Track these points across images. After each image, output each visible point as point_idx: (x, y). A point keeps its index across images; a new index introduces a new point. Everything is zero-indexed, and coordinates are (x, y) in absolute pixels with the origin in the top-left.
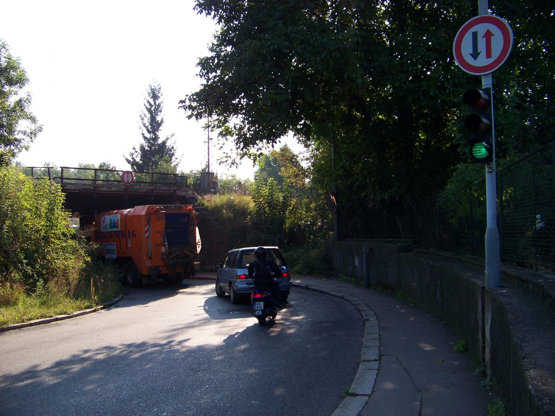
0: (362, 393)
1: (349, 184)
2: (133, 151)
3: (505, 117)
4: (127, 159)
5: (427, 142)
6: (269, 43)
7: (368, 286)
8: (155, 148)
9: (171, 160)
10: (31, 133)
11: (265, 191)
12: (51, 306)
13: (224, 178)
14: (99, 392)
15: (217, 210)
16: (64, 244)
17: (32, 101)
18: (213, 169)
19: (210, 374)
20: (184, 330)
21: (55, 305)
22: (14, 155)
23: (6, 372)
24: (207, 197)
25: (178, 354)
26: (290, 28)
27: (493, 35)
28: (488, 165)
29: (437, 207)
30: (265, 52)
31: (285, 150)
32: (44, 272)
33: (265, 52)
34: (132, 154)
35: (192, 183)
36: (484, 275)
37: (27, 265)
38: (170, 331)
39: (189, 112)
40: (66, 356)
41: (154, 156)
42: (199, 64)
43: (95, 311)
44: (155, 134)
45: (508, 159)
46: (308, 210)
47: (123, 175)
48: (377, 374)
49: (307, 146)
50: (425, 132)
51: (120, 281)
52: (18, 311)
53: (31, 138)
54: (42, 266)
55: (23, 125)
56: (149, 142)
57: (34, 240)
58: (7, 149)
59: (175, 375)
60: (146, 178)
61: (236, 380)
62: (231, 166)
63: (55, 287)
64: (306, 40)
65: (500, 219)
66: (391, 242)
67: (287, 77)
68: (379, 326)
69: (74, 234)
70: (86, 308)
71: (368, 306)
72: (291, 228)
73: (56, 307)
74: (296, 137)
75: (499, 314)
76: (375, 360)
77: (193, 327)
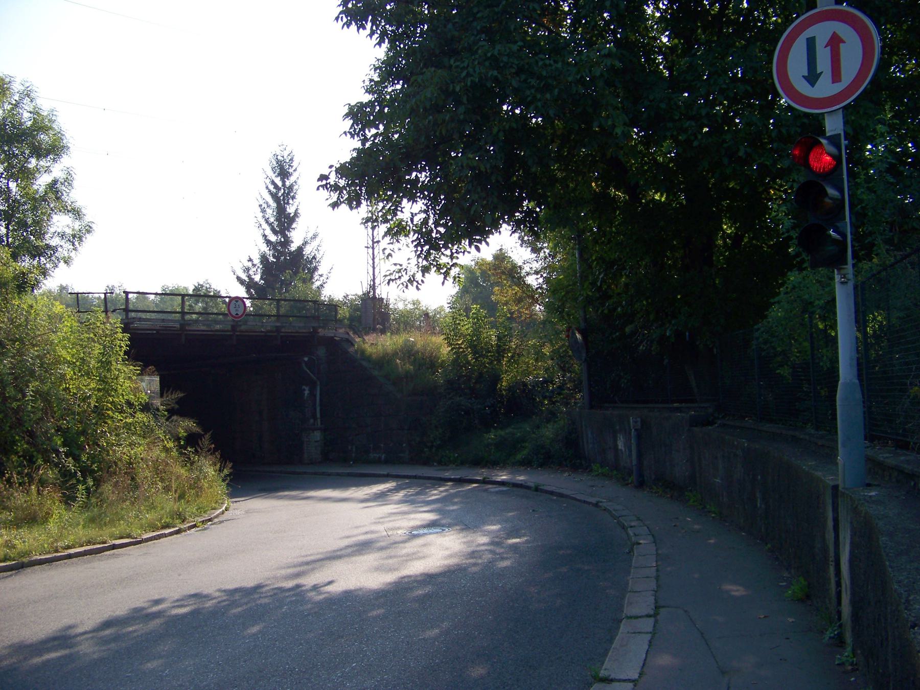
0: (622, 677)
1: (606, 311)
2: (250, 264)
3: (868, 188)
4: (239, 278)
5: (737, 238)
6: (464, 74)
7: (641, 484)
8: (285, 259)
9: (312, 277)
10: (74, 236)
11: (466, 327)
12: (105, 524)
13: (401, 306)
14: (167, 675)
15: (384, 361)
16: (130, 420)
17: (75, 184)
18: (383, 291)
19: (361, 643)
20: (325, 562)
21: (112, 522)
22: (45, 273)
23: (16, 640)
24: (370, 338)
25: (309, 606)
26: (498, 47)
27: (844, 42)
28: (839, 270)
29: (754, 347)
30: (458, 89)
31: (501, 257)
32: (95, 467)
33: (458, 89)
34: (247, 270)
35: (347, 315)
36: (837, 464)
37: (67, 456)
38: (300, 566)
39: (334, 197)
40: (121, 610)
41: (282, 271)
42: (347, 115)
43: (178, 532)
44: (285, 236)
45: (875, 260)
46: (539, 356)
47: (230, 301)
48: (650, 642)
49: (535, 250)
50: (733, 220)
51: (224, 480)
52: (49, 534)
53: (73, 245)
54: (92, 458)
55: (60, 222)
56: (275, 248)
57: (78, 414)
58: (35, 262)
59: (301, 644)
60: (269, 307)
61: (405, 652)
62: (407, 287)
63: (113, 493)
64: (526, 67)
65: (863, 366)
66: (678, 410)
67: (495, 130)
68: (657, 554)
69: (147, 404)
70: (164, 527)
71: (639, 519)
72: (510, 389)
73: (115, 527)
74: (517, 235)
75: (865, 534)
76: (648, 616)
77: (340, 557)
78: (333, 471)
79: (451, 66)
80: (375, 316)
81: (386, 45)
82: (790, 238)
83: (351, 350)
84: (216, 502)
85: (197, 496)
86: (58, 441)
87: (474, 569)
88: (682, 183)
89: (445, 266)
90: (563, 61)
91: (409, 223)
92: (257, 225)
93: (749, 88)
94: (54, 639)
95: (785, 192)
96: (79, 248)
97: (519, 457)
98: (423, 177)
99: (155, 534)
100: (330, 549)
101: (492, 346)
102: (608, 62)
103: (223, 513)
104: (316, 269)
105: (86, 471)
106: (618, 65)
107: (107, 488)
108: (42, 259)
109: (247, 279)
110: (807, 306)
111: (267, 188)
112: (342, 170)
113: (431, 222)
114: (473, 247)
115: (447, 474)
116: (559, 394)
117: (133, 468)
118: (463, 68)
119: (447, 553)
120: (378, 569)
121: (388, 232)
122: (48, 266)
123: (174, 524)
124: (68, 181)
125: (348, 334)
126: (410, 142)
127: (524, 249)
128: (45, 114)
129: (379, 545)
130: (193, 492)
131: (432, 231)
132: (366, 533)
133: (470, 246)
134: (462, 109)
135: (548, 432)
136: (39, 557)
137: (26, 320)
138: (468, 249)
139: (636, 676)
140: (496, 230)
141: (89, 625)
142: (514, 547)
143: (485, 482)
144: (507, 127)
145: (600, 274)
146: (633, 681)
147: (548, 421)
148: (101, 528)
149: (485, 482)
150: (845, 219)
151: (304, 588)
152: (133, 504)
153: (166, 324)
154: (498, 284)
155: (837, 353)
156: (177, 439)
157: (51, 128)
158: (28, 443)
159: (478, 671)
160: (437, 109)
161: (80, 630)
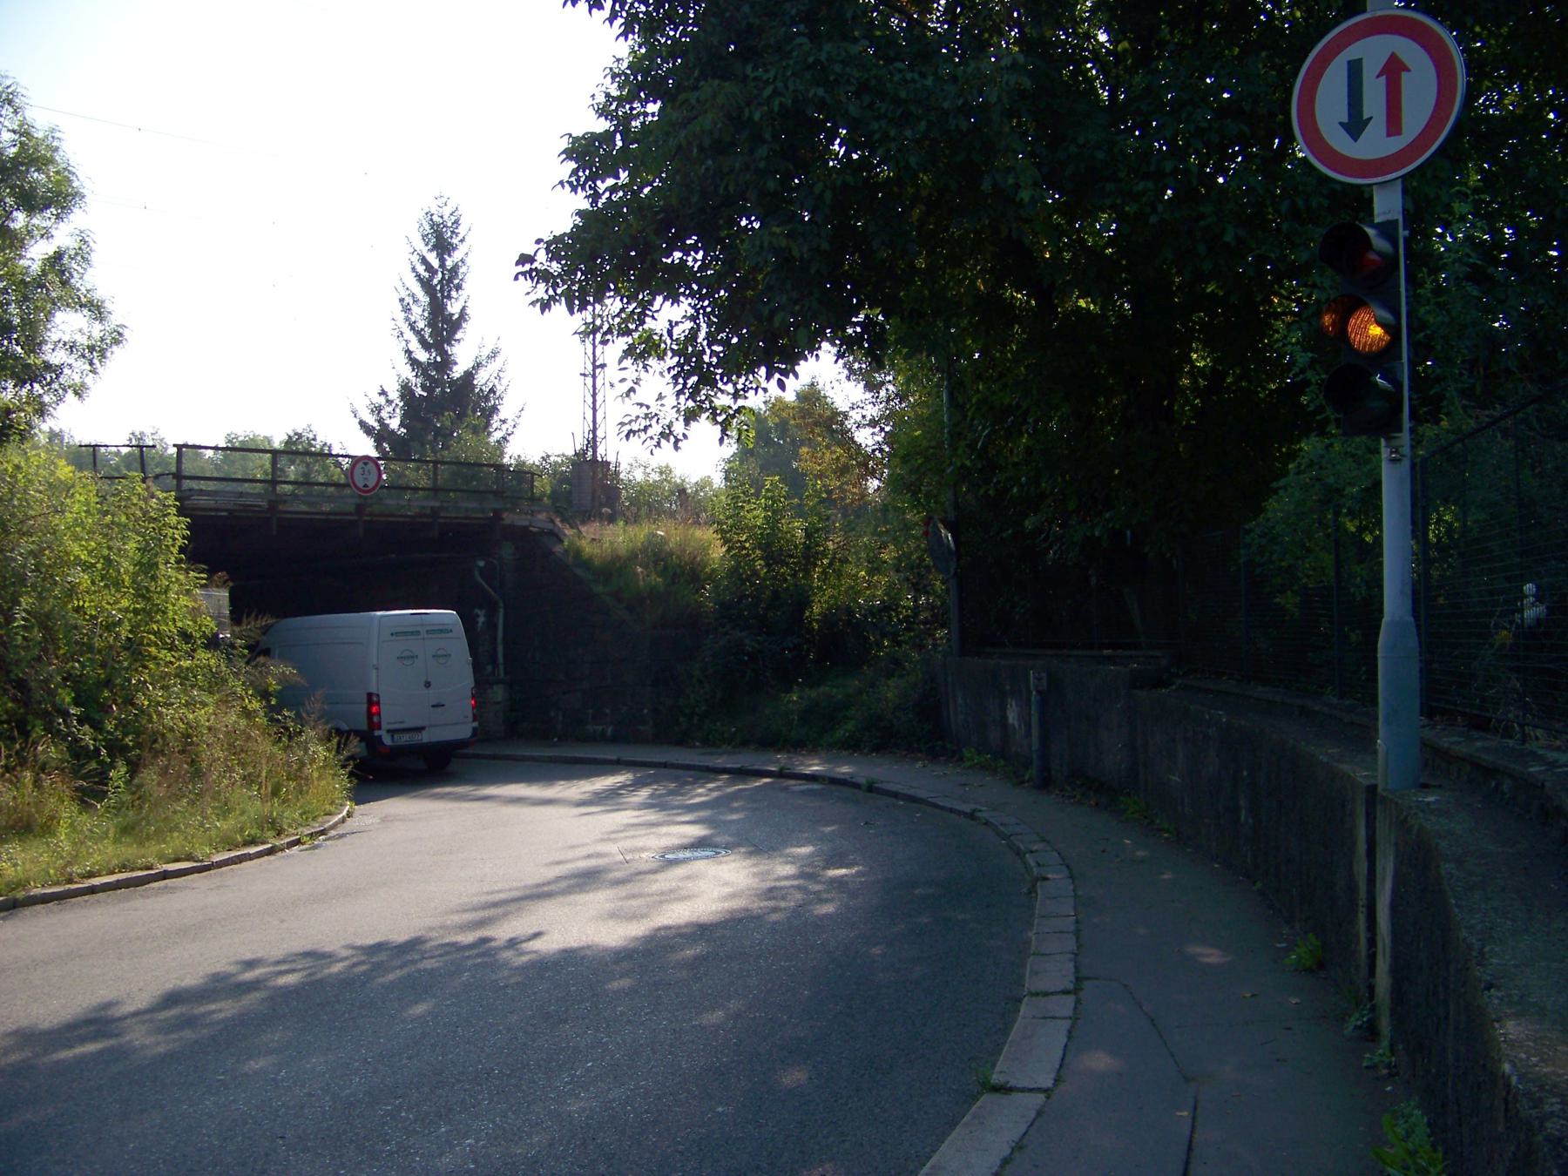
0: (1027, 1084)
2: (382, 400)
3: (1438, 304)
4: (362, 424)
5: (1215, 376)
6: (768, 91)
7: (1045, 783)
8: (443, 391)
9: (488, 424)
10: (92, 349)
11: (756, 515)
12: (148, 838)
13: (639, 476)
15: (615, 569)
16: (186, 663)
17: (94, 257)
21: (160, 835)
22: (42, 411)
23: (24, 1023)
24: (589, 530)
25: (506, 973)
26: (827, 47)
27: (1408, 70)
28: (1388, 439)
30: (757, 117)
32: (129, 740)
33: (757, 117)
34: (377, 410)
35: (548, 490)
36: (1375, 752)
37: (81, 721)
39: (541, 291)
43: (271, 851)
44: (443, 353)
45: (1445, 424)
46: (875, 567)
47: (353, 466)
48: (1070, 1032)
49: (872, 387)
50: (1209, 345)
53: (91, 364)
54: (121, 724)
55: (67, 325)
57: (100, 652)
58: (24, 392)
59: (500, 1032)
60: (416, 475)
61: (671, 1045)
62: (658, 445)
64: (873, 82)
65: (1421, 595)
68: (1076, 896)
70: (247, 844)
72: (826, 618)
75: (1418, 860)
76: (1066, 992)
78: (487, 752)
79: (746, 77)
80: (594, 492)
81: (634, 39)
82: (1307, 383)
83: (558, 549)
84: (332, 803)
85: (301, 792)
86: (66, 696)
87: (775, 917)
88: (1126, 282)
89: (725, 409)
90: (935, 74)
91: (666, 336)
92: (396, 333)
93: (1245, 128)
94: (89, 1022)
95: (1298, 301)
96: (100, 370)
97: (840, 734)
98: (695, 260)
99: (233, 854)
100: (530, 882)
101: (796, 547)
102: (1013, 79)
103: (343, 821)
104: (495, 409)
105: (116, 749)
106: (1027, 83)
107: (149, 776)
108: (36, 386)
109: (376, 425)
110: (1331, 497)
111: (414, 269)
112: (555, 247)
113: (702, 335)
114: (774, 382)
115: (720, 761)
116: (908, 629)
117: (192, 743)
118: (767, 83)
119: (727, 890)
120: (614, 915)
121: (629, 352)
122: (46, 399)
123: (265, 838)
124: (82, 254)
125: (552, 521)
126: (674, 201)
127: (853, 383)
128: (40, 135)
129: (611, 876)
130: (292, 784)
131: (703, 352)
132: (589, 856)
133: (768, 378)
134: (762, 152)
135: (891, 691)
136: (39, 891)
137: (11, 491)
138: (764, 384)
139: (1049, 1083)
140: (811, 353)
141: (141, 1001)
142: (839, 883)
143: (781, 775)
144: (839, 182)
145: (984, 429)
146: (1046, 1091)
147: (889, 675)
148: (141, 844)
149: (781, 775)
150: (1400, 358)
151: (493, 944)
152: (192, 803)
153: (243, 501)
154: (810, 442)
155: (1380, 572)
156: (264, 695)
157: (51, 161)
158: (14, 700)
159: (794, 1077)
160: (720, 148)
161: (129, 1008)
